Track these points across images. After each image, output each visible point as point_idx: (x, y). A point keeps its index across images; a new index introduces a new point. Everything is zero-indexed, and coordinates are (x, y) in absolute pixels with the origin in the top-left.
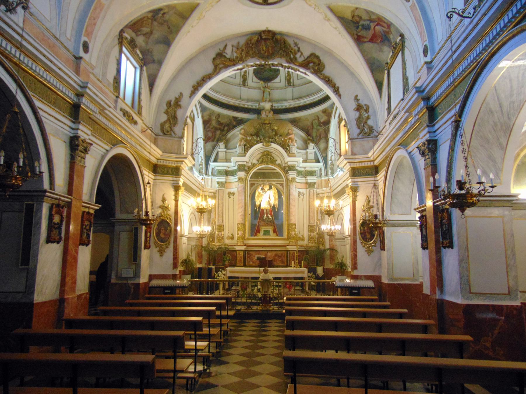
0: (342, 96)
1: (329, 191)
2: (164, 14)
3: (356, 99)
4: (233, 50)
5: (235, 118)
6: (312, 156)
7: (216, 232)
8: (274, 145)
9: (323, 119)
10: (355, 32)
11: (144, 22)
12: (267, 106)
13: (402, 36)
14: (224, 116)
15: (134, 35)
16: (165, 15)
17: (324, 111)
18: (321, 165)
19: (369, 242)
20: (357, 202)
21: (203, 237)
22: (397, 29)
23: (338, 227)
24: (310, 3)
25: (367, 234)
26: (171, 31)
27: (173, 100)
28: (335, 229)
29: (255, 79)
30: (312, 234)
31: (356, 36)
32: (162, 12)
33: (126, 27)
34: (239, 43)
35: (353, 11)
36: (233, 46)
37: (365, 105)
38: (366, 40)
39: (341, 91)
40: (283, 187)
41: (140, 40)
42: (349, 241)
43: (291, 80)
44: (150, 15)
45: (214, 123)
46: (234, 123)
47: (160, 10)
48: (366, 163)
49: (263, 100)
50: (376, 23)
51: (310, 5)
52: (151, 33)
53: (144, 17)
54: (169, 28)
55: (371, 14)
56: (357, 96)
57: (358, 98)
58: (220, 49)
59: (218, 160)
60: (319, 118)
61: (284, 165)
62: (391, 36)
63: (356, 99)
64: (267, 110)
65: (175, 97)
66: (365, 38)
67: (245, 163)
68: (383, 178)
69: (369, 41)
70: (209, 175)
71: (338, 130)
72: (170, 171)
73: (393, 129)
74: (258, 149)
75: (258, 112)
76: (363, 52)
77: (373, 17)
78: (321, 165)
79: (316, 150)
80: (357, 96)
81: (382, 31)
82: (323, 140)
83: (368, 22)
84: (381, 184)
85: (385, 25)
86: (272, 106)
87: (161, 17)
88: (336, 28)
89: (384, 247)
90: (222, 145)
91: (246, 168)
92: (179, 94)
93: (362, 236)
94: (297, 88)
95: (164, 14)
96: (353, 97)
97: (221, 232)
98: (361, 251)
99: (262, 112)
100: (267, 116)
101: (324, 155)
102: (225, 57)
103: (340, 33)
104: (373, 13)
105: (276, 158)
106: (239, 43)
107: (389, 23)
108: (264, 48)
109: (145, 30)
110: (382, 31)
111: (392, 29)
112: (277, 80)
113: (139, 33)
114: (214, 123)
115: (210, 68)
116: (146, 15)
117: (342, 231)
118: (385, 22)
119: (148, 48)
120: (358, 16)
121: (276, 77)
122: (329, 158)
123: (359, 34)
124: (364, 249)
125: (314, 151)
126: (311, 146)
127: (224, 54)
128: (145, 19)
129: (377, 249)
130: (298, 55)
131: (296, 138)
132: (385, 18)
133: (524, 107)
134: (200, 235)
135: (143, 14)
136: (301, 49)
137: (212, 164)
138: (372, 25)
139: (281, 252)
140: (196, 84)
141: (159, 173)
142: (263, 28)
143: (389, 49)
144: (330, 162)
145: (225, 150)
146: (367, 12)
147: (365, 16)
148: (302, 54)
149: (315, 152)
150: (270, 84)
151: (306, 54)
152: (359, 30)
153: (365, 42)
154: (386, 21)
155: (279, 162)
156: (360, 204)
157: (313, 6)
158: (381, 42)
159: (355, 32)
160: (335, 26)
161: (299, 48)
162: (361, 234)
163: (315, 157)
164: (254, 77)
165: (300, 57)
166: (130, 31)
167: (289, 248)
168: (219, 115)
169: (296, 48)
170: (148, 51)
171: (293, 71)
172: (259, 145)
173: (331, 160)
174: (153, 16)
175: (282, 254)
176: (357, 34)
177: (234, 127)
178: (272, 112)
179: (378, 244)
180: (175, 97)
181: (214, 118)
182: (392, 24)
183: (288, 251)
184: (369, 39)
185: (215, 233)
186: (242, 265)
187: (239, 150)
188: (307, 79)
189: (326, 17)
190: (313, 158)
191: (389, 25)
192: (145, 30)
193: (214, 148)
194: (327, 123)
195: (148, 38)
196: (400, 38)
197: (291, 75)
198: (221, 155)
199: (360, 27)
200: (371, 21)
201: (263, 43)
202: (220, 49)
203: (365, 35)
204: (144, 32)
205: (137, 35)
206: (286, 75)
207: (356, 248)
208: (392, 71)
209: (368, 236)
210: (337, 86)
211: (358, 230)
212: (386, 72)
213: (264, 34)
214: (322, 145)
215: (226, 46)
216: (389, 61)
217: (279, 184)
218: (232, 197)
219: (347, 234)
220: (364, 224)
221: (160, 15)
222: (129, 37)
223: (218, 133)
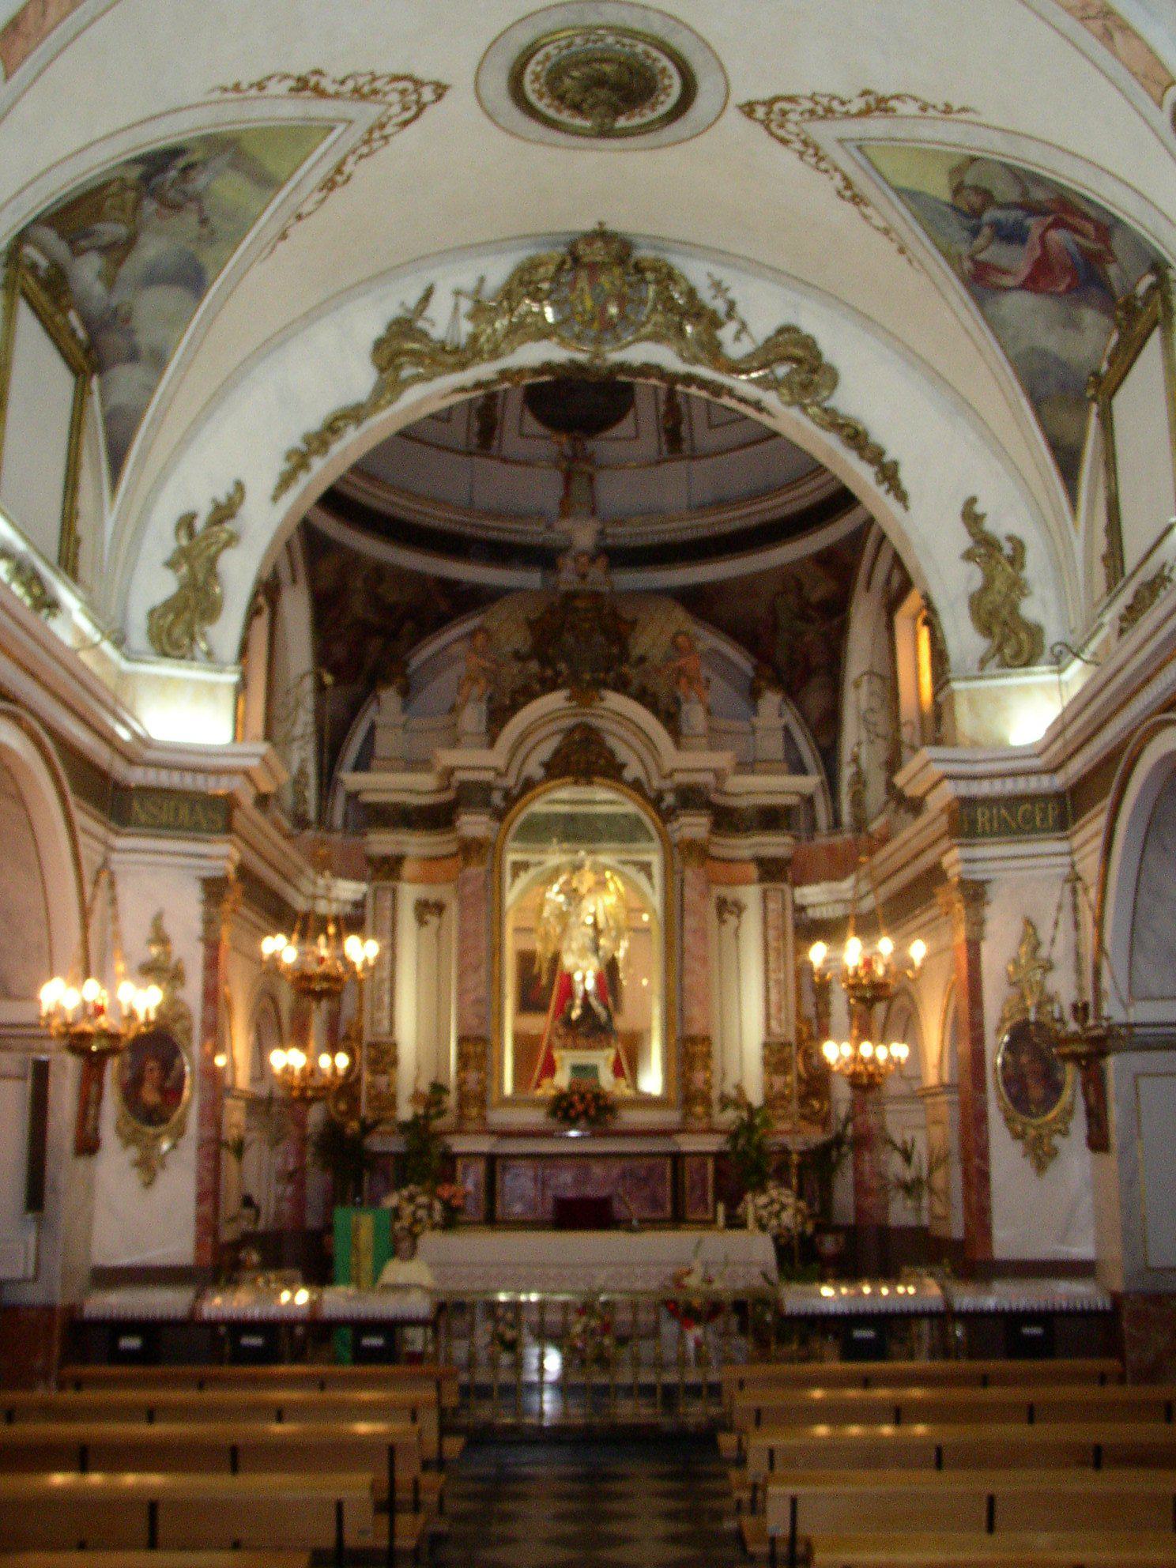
0: (913, 501)
1: (849, 895)
2: (190, 167)
3: (971, 517)
4: (456, 308)
5: (447, 586)
6: (774, 746)
7: (367, 1077)
8: (615, 701)
9: (820, 590)
10: (964, 249)
11: (109, 203)
12: (584, 535)
13: (1158, 267)
14: (404, 576)
15: (61, 249)
16: (193, 174)
17: (825, 559)
18: (811, 782)
19: (1037, 1116)
20: (985, 949)
21: (309, 1102)
22: (1139, 245)
23: (900, 1051)
24: (781, 133)
25: (1030, 1082)
26: (213, 232)
27: (204, 511)
28: (890, 1058)
29: (533, 426)
30: (778, 1081)
31: (967, 265)
32: (181, 163)
33: (36, 221)
34: (482, 280)
35: (957, 171)
36: (458, 293)
37: (1010, 538)
38: (1007, 281)
39: (907, 477)
40: (650, 876)
41: (87, 271)
42: (946, 1109)
43: (684, 428)
44: (135, 173)
45: (358, 606)
46: (444, 606)
47: (174, 153)
48: (200, 778)
49: (566, 508)
50: (1050, 219)
51: (784, 142)
52: (129, 244)
53: (105, 186)
54: (204, 222)
55: (1028, 184)
56: (972, 501)
57: (979, 509)
58: (402, 304)
59: (374, 763)
60: (799, 586)
61: (656, 783)
62: (1113, 271)
63: (971, 517)
64: (583, 553)
65: (214, 500)
66: (1005, 272)
67: (489, 776)
68: (1099, 842)
69: (1023, 286)
70: (330, 829)
71: (884, 640)
72: (184, 812)
73: (1146, 641)
74: (547, 718)
75: (544, 557)
76: (994, 324)
77: (1039, 195)
78: (811, 782)
79: (790, 717)
80: (972, 501)
81: (1073, 248)
82: (817, 682)
83: (1017, 214)
84: (1089, 866)
85: (1089, 228)
86: (601, 533)
87: (174, 183)
88: (886, 232)
89: (1105, 1137)
90: (389, 697)
91: (497, 798)
92: (229, 487)
93: (1008, 1091)
94: (705, 463)
95: (190, 167)
96: (958, 507)
97: (384, 1072)
98: (1005, 1154)
99: (560, 561)
100: (584, 576)
101: (825, 741)
102: (424, 335)
103: (902, 251)
104: (1038, 180)
105: (623, 754)
106: (482, 280)
107: (1107, 221)
108: (589, 304)
109: (111, 230)
110: (1073, 248)
111: (1118, 243)
112: (625, 428)
113: (84, 243)
114: (358, 606)
115: (362, 380)
116: (115, 175)
117: (909, 1072)
118: (1085, 217)
119: (114, 302)
120: (976, 189)
121: (619, 418)
122: (846, 753)
123: (981, 257)
124: (1018, 1147)
125: (783, 722)
126: (771, 701)
127: (421, 324)
128: (113, 189)
129: (1073, 1146)
130: (726, 334)
131: (705, 672)
132: (1088, 201)
133: (668, 8)
134: (303, 1090)
135: (107, 171)
136: (740, 309)
137: (350, 780)
138: (1034, 225)
139: (647, 1162)
140: (303, 447)
141: (138, 824)
142: (589, 225)
143: (1105, 321)
144: (847, 773)
145: (403, 718)
146: (1021, 177)
147: (1006, 191)
148: (743, 327)
149: (786, 729)
150: (592, 445)
151: (762, 328)
152: (980, 241)
153: (1007, 289)
154: (1092, 213)
155: (633, 771)
156: (998, 954)
157: (798, 146)
158: (1069, 289)
159: (964, 249)
160: (881, 224)
161: (731, 306)
162: (1007, 1081)
163: (787, 752)
164: (529, 418)
165: (737, 338)
166: (49, 236)
167: (689, 1144)
168: (380, 572)
169: (720, 306)
170: (115, 312)
171: (704, 394)
172: (555, 700)
173: (855, 759)
174: (146, 179)
175: (650, 1169)
176: (972, 258)
177: (441, 622)
178: (602, 562)
179: (1079, 1126)
180: (214, 500)
181: (359, 584)
182: (1117, 221)
183: (677, 1157)
184: (1021, 278)
185: (358, 1079)
186: (688, 1160)
187: (473, 717)
188: (767, 428)
189: (849, 185)
190: (780, 755)
191: (1106, 226)
192: (111, 230)
193: (354, 709)
194: (837, 610)
195: (119, 263)
196: (1149, 279)
197: (684, 409)
198: (385, 744)
199: (986, 231)
200: (1032, 209)
201: (583, 283)
202: (402, 304)
203: (1004, 263)
204: (106, 239)
205: (77, 252)
206: (663, 408)
207: (986, 1146)
208: (1120, 402)
209: (1036, 1092)
210: (887, 459)
211: (995, 1059)
212: (1094, 408)
213: (590, 245)
214: (816, 701)
215: (428, 294)
216: (1105, 367)
217: (635, 863)
218: (433, 920)
219: (931, 1078)
220: (1022, 1035)
221: (173, 174)
222: (43, 263)
223: (375, 645)
